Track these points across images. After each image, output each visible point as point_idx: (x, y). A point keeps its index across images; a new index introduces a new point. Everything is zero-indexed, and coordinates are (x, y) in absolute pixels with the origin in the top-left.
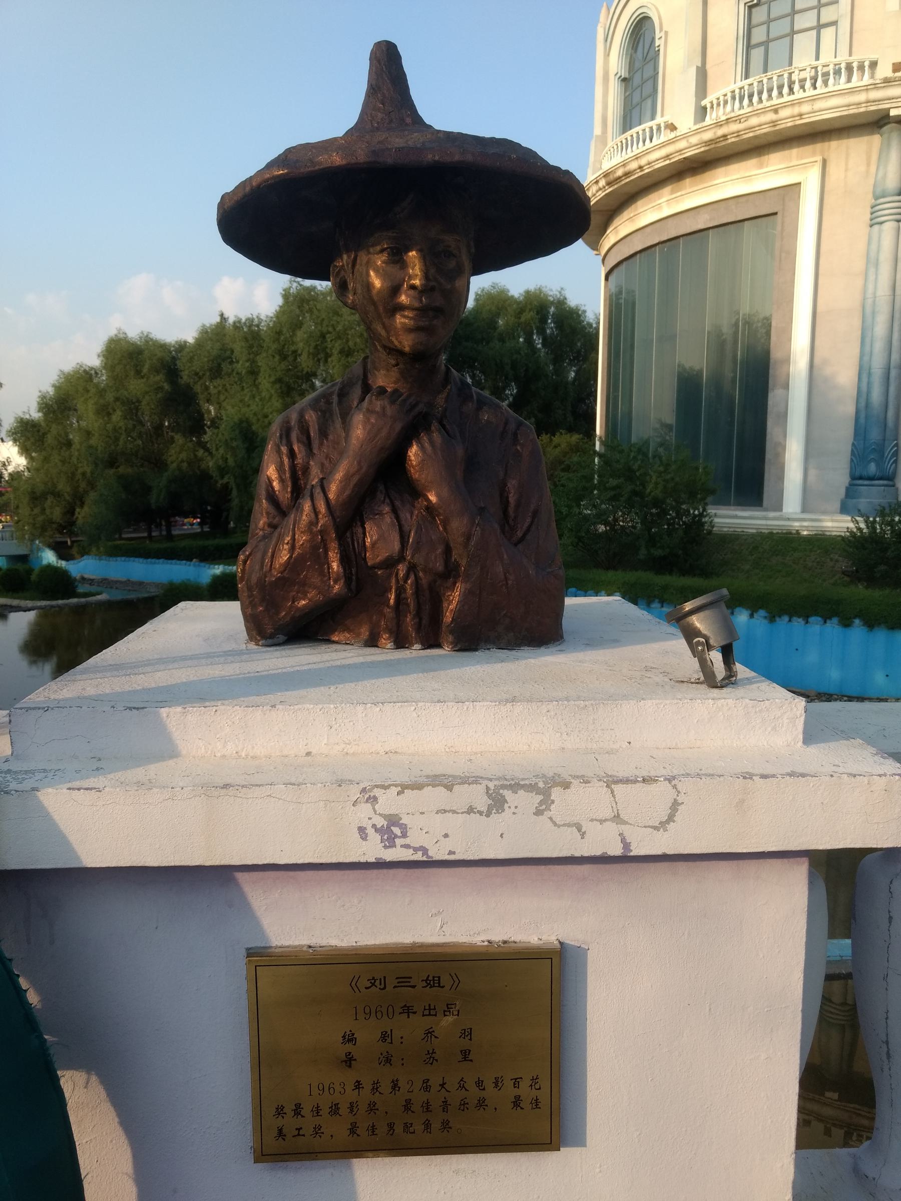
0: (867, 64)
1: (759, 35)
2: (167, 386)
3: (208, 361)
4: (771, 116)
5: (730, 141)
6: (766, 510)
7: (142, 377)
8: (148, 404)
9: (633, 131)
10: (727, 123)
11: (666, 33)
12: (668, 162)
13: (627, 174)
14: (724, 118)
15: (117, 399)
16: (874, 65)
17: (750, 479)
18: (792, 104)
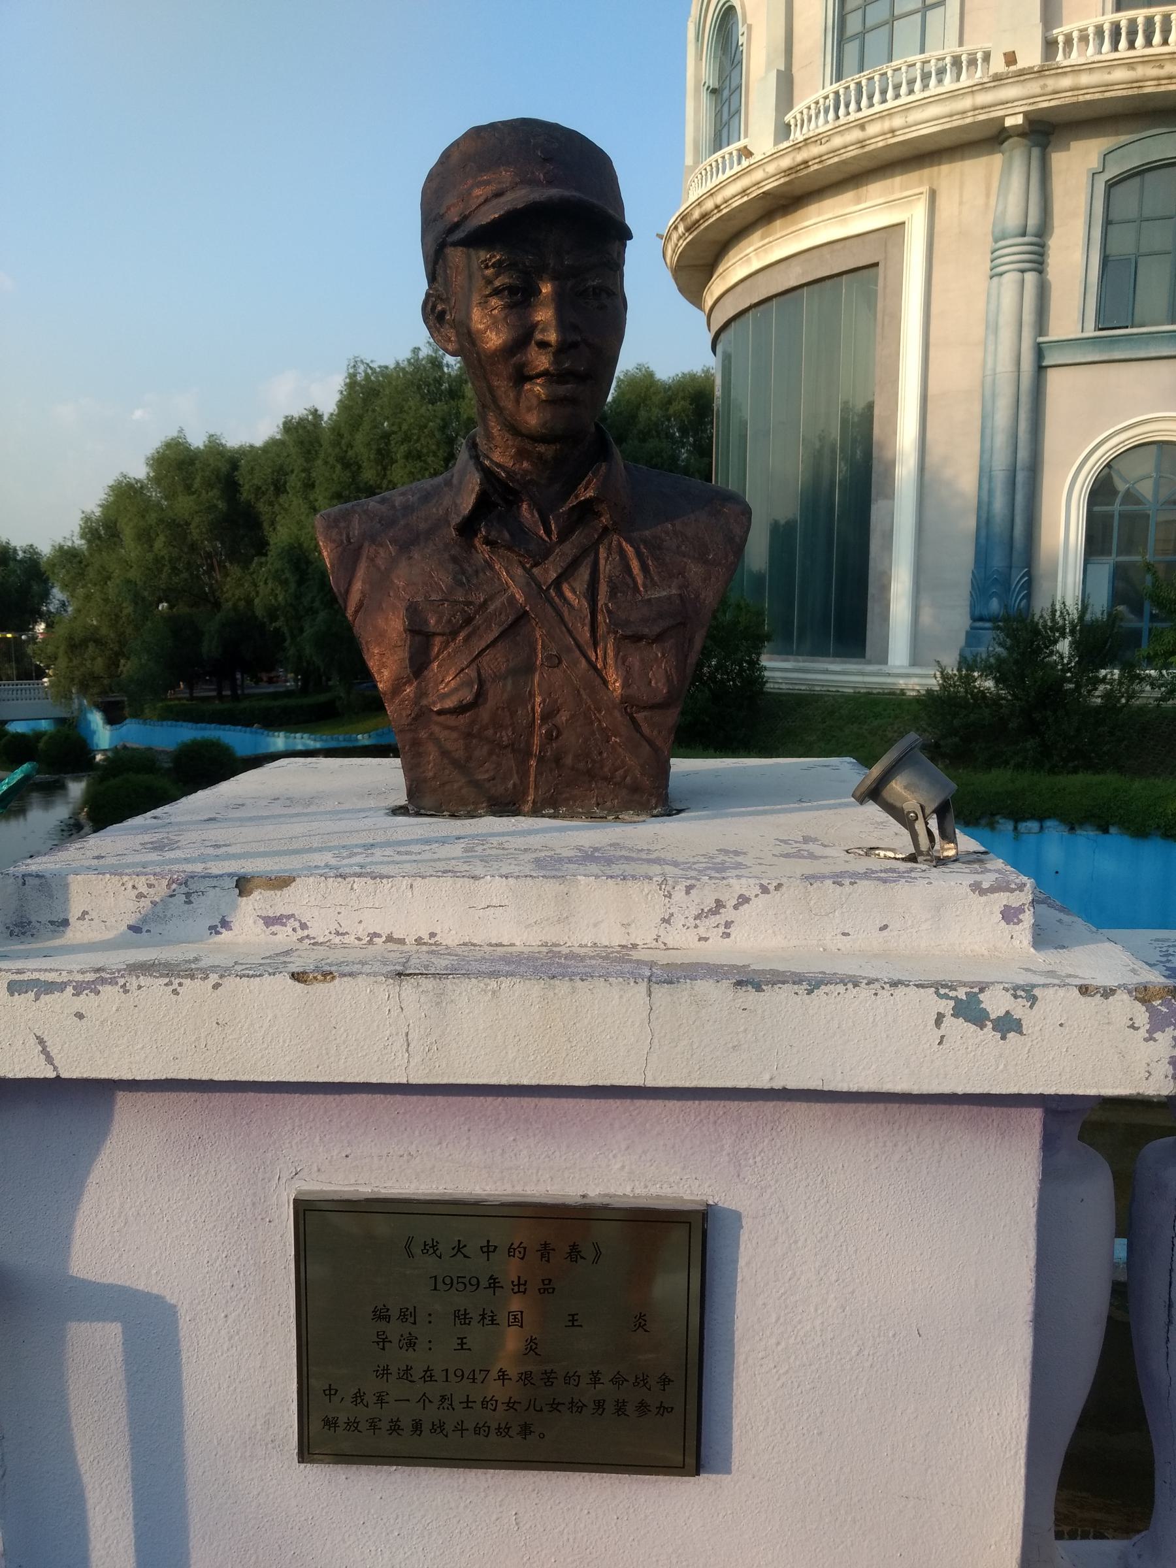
0: (979, 56)
1: (854, 24)
2: (221, 505)
3: (273, 473)
4: (856, 135)
5: (812, 169)
6: (870, 663)
7: (194, 493)
8: (198, 526)
10: (806, 145)
11: (750, 27)
12: (745, 199)
13: (705, 216)
14: (801, 138)
15: (161, 521)
16: (987, 57)
17: (847, 623)
18: (881, 116)
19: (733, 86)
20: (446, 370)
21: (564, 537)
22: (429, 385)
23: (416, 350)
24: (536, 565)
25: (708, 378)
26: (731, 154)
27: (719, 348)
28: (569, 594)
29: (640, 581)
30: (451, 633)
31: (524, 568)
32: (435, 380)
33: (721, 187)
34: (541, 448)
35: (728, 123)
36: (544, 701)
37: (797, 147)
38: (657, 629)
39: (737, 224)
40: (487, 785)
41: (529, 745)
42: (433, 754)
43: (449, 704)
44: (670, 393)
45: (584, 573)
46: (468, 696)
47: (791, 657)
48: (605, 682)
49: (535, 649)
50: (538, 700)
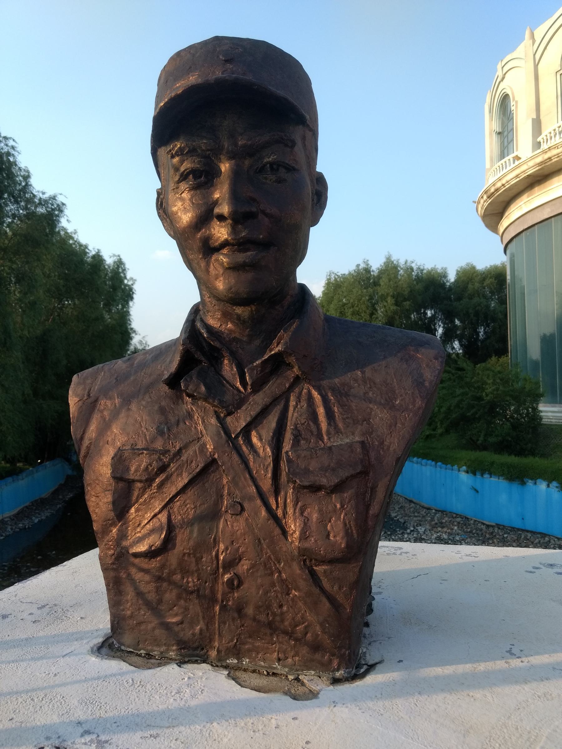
5: (553, 161)
9: (506, 159)
10: (550, 150)
11: (517, 102)
12: (518, 179)
13: (497, 190)
19: (509, 129)
20: (372, 273)
21: (258, 386)
22: (364, 281)
23: (358, 266)
24: (229, 414)
25: (504, 267)
26: (509, 160)
27: (508, 252)
28: (255, 440)
29: (324, 425)
30: (147, 480)
31: (218, 418)
32: (367, 278)
33: (505, 175)
34: (239, 310)
35: (507, 146)
36: (226, 549)
37: (545, 152)
38: (335, 480)
39: (515, 192)
40: (176, 629)
41: (213, 591)
42: (130, 594)
43: (142, 548)
44: (484, 275)
45: (272, 422)
46: (156, 540)
47: (557, 405)
48: (284, 533)
49: (222, 496)
50: (222, 546)
